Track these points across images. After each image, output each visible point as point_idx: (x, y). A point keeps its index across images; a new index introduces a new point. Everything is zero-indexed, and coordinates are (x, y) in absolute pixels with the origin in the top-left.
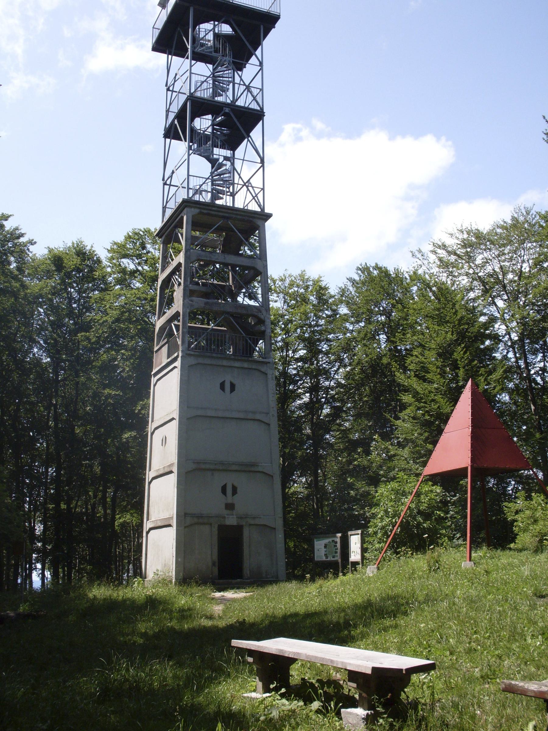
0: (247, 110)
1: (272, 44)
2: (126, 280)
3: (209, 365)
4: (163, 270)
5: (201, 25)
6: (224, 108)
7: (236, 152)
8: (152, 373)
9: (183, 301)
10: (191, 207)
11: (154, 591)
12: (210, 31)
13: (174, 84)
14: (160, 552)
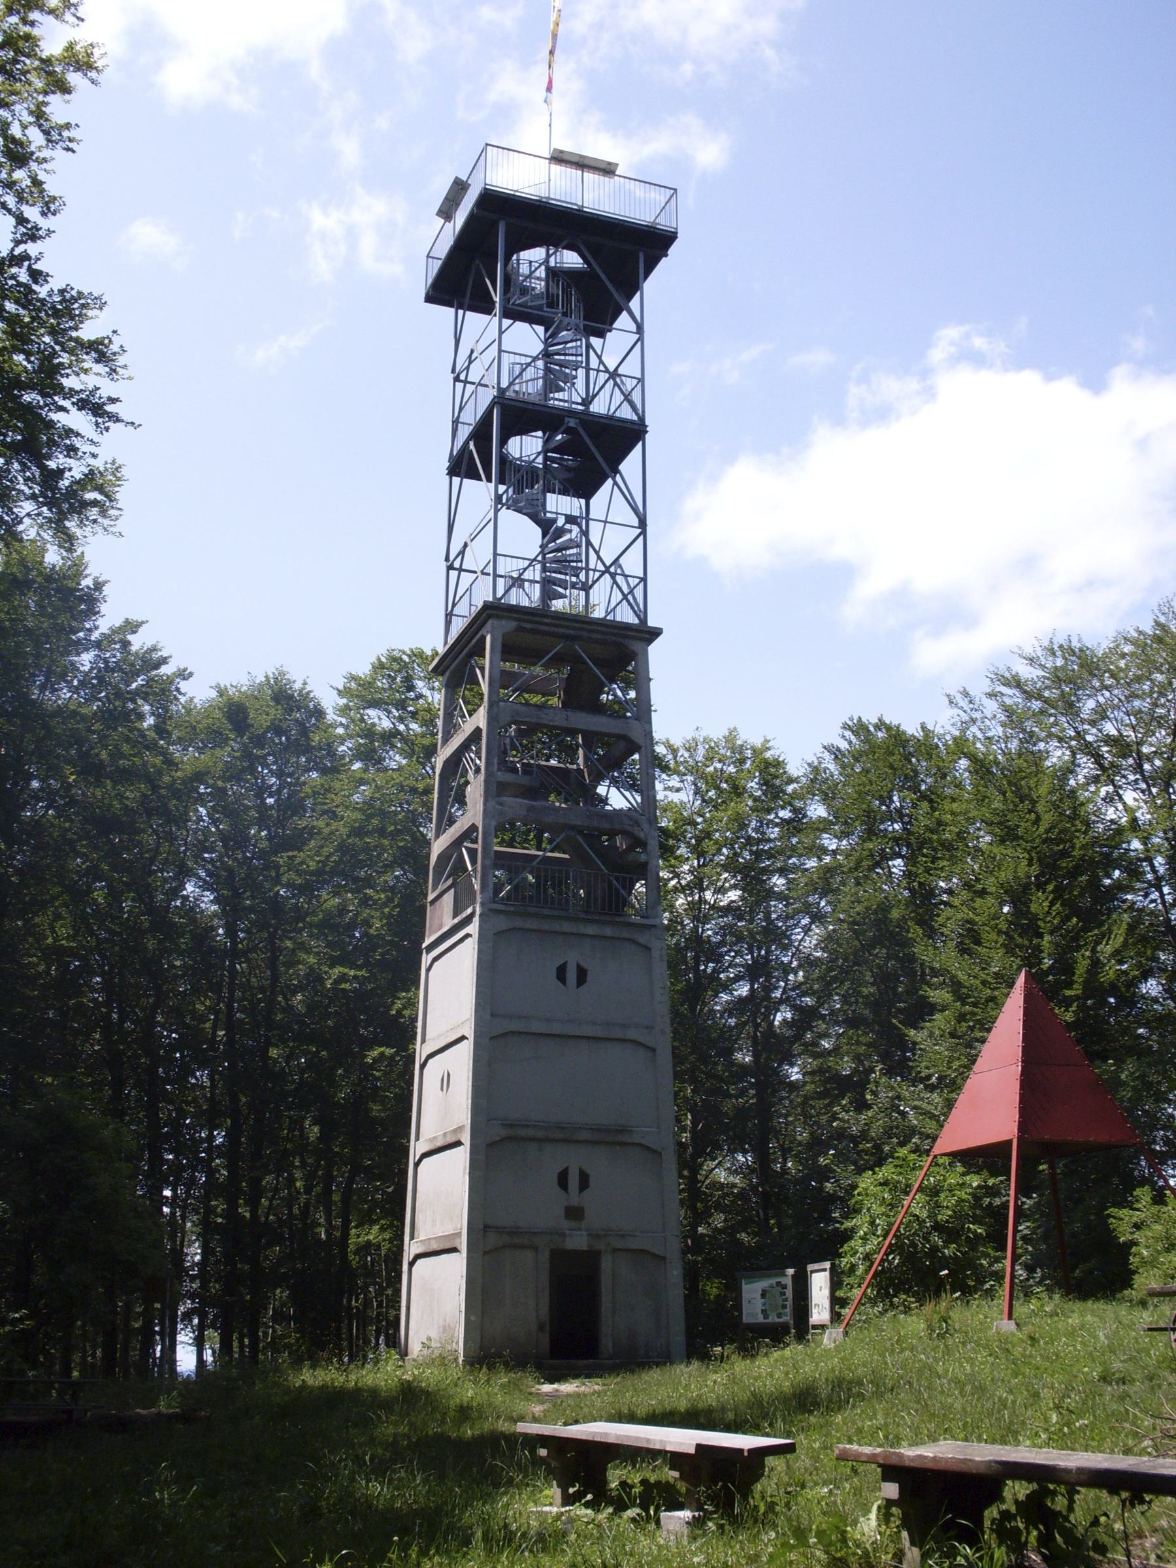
0: (613, 423)
1: (660, 288)
2: (374, 751)
3: (534, 930)
4: (446, 740)
5: (522, 253)
6: (567, 419)
7: (594, 501)
8: (424, 945)
9: (485, 804)
10: (498, 617)
11: (416, 1373)
12: (541, 265)
13: (468, 368)
14: (436, 1302)
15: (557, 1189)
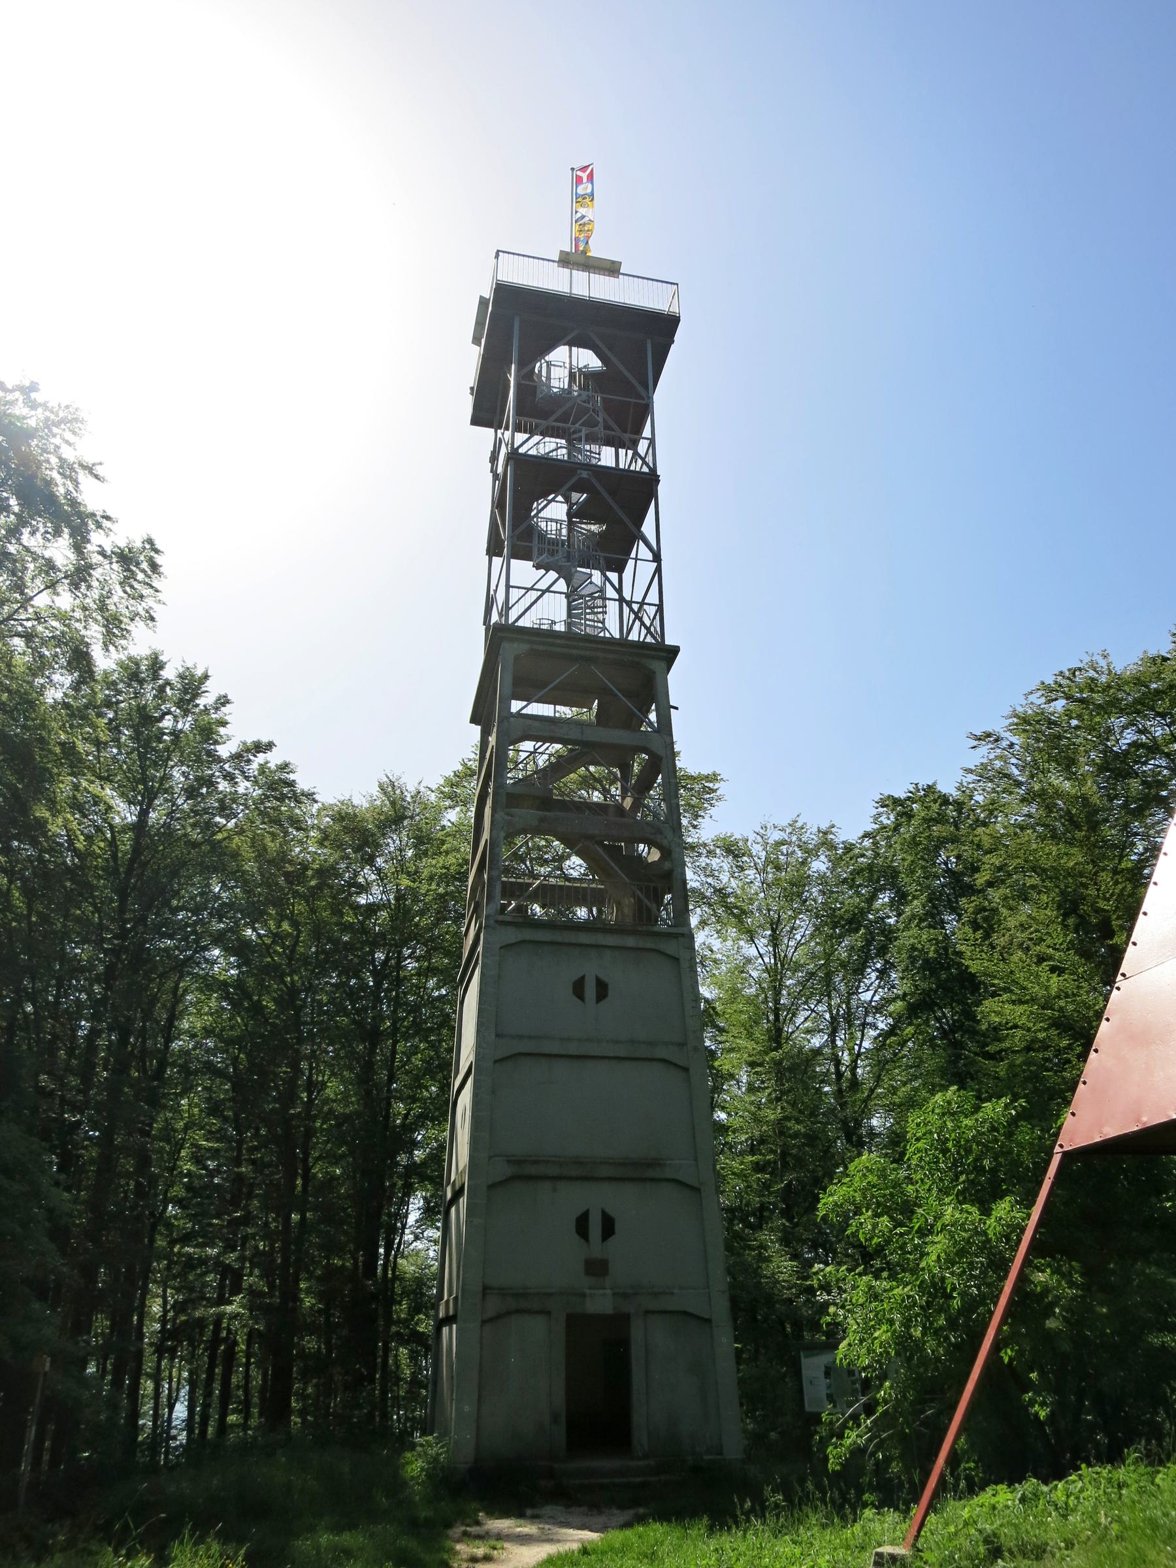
15: (576, 1239)
